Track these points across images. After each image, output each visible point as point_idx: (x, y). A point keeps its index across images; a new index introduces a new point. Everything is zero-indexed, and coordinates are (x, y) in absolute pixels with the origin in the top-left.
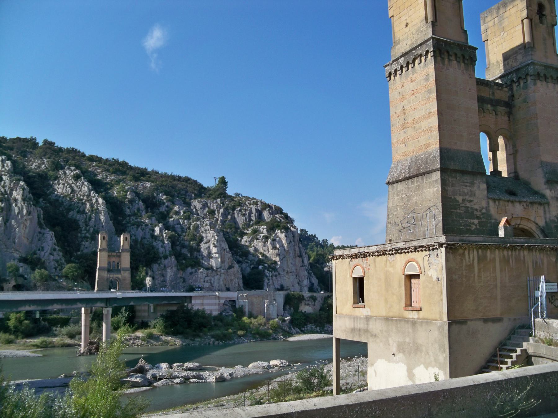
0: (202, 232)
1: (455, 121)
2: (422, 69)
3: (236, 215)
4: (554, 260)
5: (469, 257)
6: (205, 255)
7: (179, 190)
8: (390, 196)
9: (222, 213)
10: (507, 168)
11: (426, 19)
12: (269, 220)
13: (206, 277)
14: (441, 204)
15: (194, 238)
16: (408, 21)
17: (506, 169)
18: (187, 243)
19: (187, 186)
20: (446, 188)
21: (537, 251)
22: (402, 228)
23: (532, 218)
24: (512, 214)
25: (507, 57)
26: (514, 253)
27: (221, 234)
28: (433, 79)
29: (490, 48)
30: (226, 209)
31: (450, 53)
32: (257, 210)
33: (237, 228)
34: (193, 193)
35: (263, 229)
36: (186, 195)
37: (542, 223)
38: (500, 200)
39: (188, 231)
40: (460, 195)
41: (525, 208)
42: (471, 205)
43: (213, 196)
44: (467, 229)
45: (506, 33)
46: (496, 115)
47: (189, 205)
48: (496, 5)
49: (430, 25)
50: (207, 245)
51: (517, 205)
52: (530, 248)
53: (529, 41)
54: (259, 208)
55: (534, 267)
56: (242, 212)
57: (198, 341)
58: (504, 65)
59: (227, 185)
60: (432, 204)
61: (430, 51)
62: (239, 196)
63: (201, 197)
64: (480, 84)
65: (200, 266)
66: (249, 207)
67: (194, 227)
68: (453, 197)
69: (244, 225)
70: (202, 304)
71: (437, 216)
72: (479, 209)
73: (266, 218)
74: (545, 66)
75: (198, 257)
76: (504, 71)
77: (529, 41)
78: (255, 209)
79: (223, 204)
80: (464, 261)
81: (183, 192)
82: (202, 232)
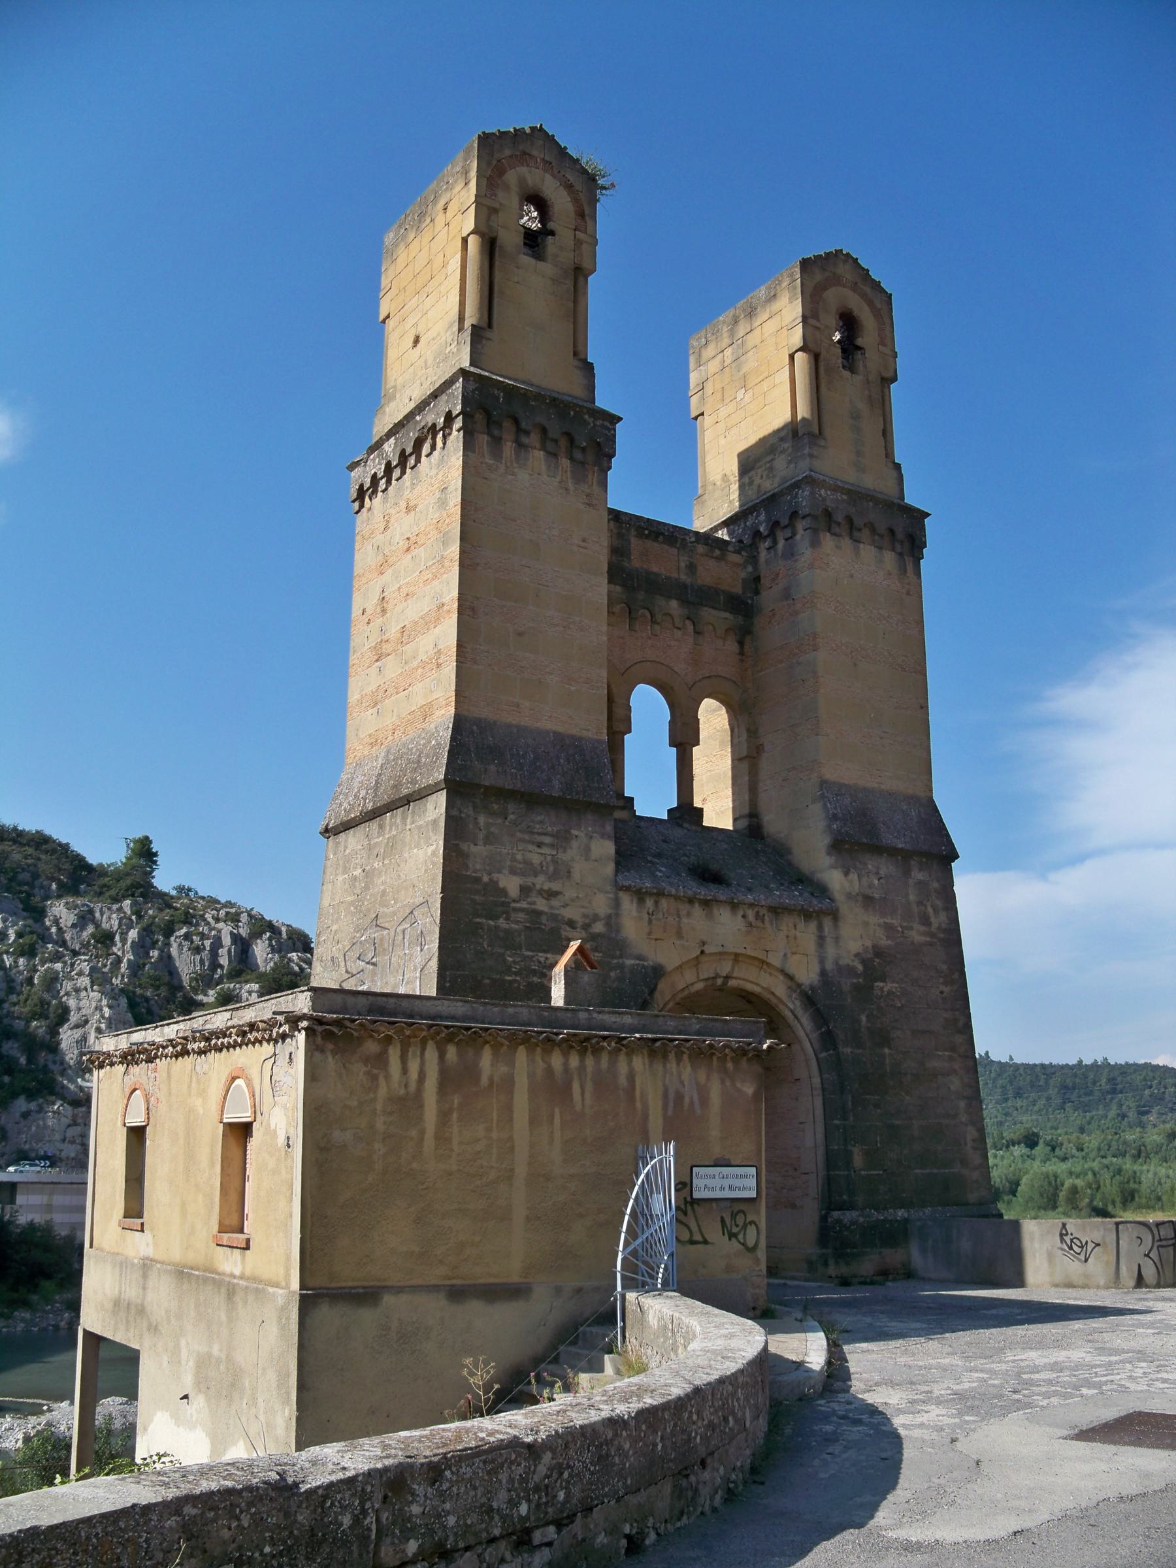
0: (67, 994)
1: (520, 634)
2: (434, 472)
3: (174, 951)
4: (749, 1089)
5: (405, 1071)
6: (72, 1062)
7: (13, 870)
8: (329, 871)
9: (133, 942)
10: (734, 801)
11: (461, 319)
12: (268, 968)
13: (69, 1126)
14: (439, 896)
15: (41, 1010)
16: (421, 330)
17: (731, 805)
18: (19, 1024)
19: (39, 859)
20: (464, 846)
21: (685, 1057)
22: (347, 976)
23: (775, 960)
24: (704, 943)
25: (749, 463)
26: (590, 1061)
27: (124, 1001)
28: (456, 498)
29: (709, 436)
30: (147, 931)
31: (523, 425)
32: (236, 938)
33: (174, 985)
34: (53, 879)
35: (250, 993)
36: (32, 885)
37: (807, 974)
38: (660, 894)
39: (25, 989)
40: (513, 872)
41: (750, 925)
42: (551, 907)
43: (113, 892)
44: (529, 984)
45: (750, 393)
46: (698, 633)
47: (38, 913)
48: (730, 313)
49: (467, 336)
50: (78, 1033)
51: (724, 915)
52: (655, 1050)
53: (807, 415)
54: (241, 930)
55: (670, 1113)
56: (192, 942)
57: (23, 1320)
58: (742, 488)
59: (155, 862)
60: (419, 900)
61: (455, 413)
62: (187, 895)
63: (76, 893)
64: (647, 537)
65: (52, 1093)
66: (214, 929)
67: (44, 979)
68: (486, 879)
69: (197, 980)
70: (49, 1208)
71: (428, 938)
72: (580, 921)
73: (259, 961)
74: (849, 492)
75: (52, 1066)
76: (740, 506)
77: (807, 415)
78: (231, 933)
79: (140, 917)
80: (382, 1080)
81: (25, 876)
82: (67, 994)
